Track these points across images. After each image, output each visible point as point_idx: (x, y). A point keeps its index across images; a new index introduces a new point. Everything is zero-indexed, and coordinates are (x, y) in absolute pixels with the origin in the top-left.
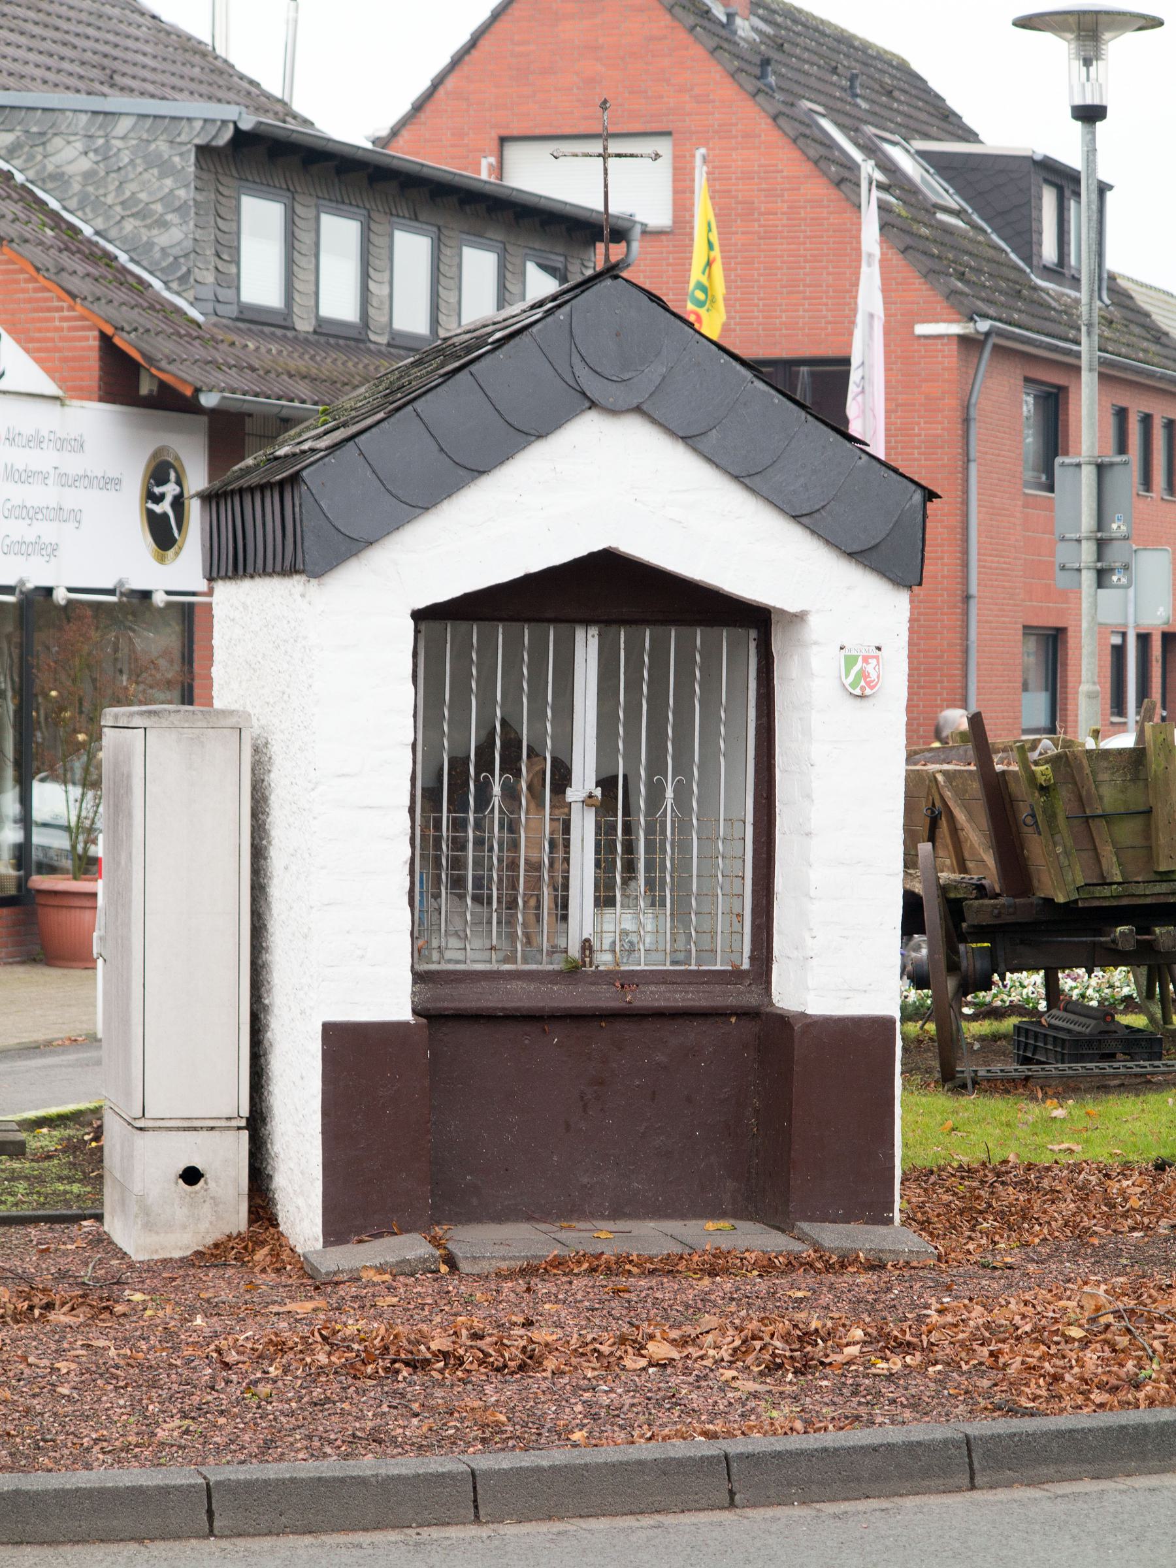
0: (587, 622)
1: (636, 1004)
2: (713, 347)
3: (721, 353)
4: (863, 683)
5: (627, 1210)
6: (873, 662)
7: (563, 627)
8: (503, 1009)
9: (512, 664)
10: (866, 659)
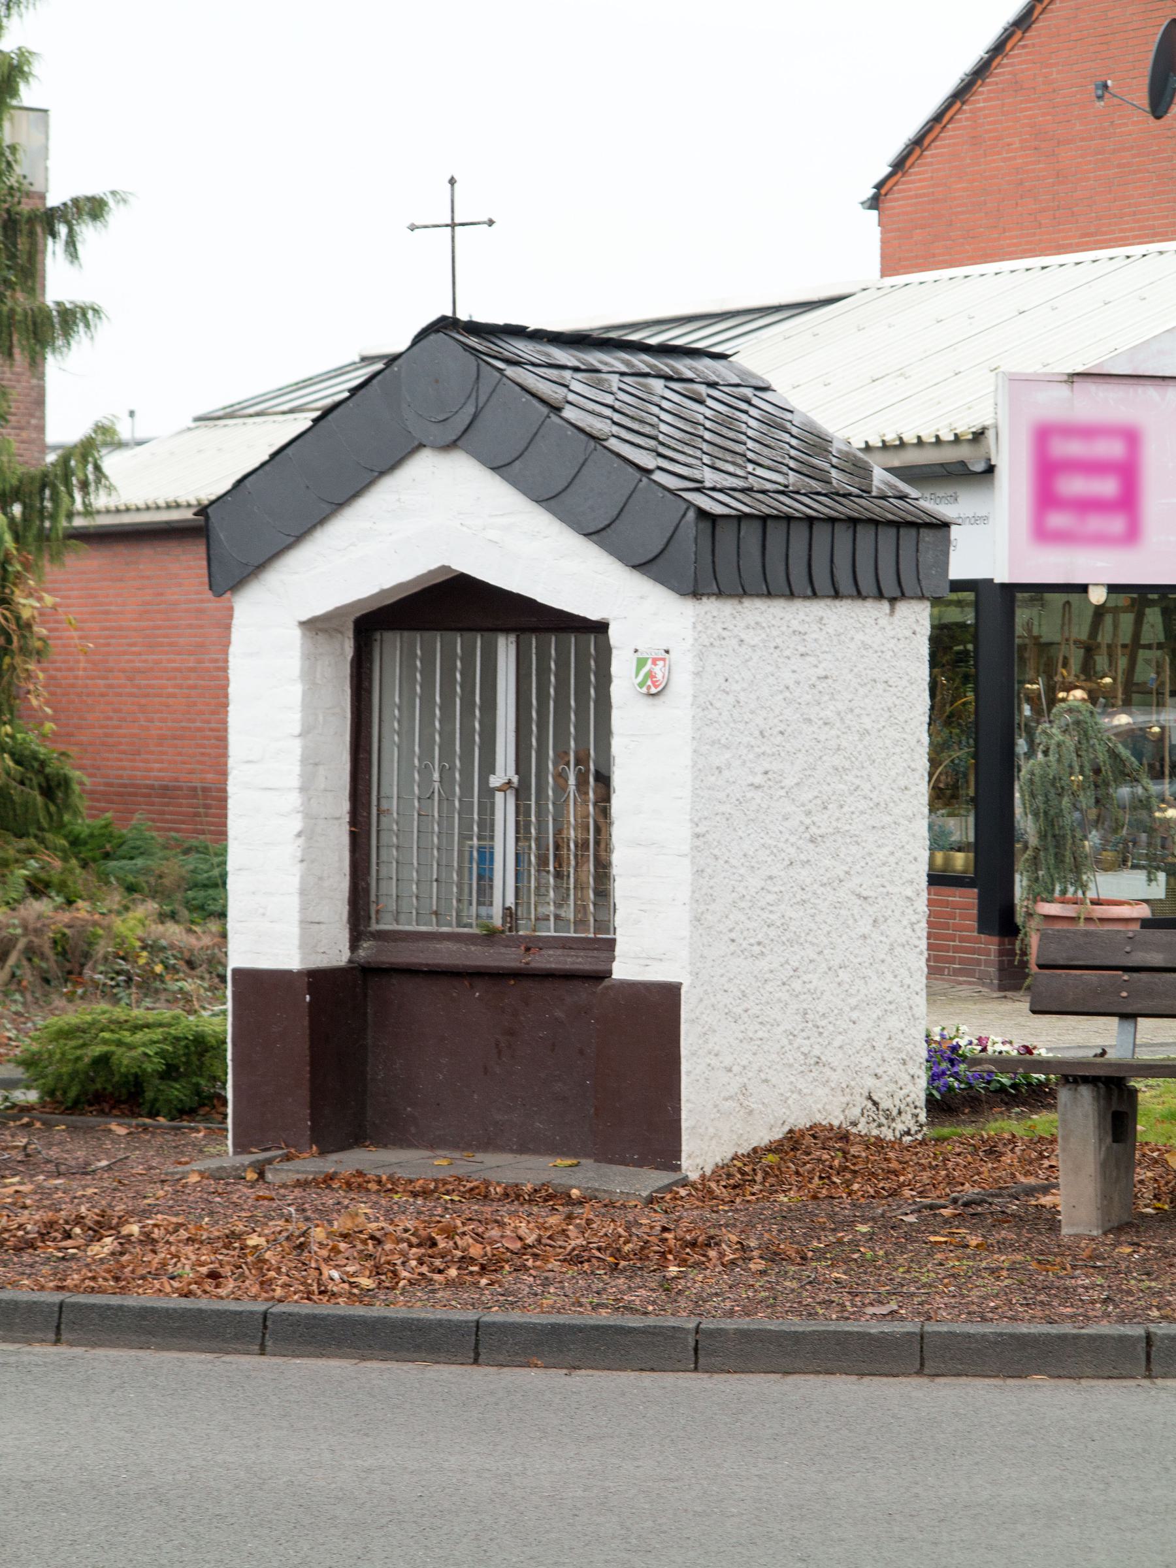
0: (507, 630)
1: (533, 965)
2: (517, 388)
3: (523, 393)
4: (649, 683)
5: (531, 1146)
6: (661, 663)
7: (486, 634)
8: (427, 965)
9: (563, 665)
10: (654, 662)
